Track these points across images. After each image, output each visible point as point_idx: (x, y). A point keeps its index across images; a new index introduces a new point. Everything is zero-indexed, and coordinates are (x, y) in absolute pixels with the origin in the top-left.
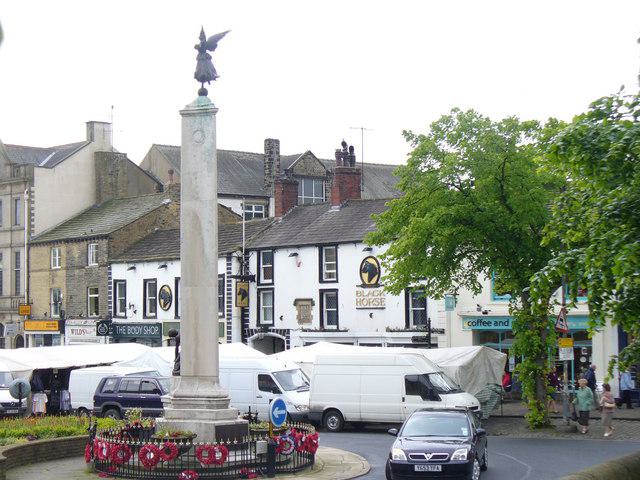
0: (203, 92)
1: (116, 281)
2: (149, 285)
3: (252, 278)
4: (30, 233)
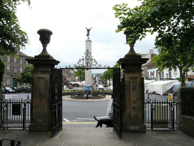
0: (88, 38)
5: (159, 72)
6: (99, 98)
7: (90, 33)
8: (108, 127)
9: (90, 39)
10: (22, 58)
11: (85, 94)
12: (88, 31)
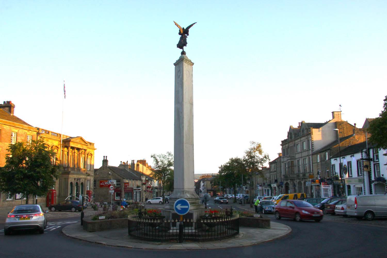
0: (183, 53)
1: (333, 166)
2: (341, 165)
3: (371, 160)
4: (312, 151)
5: (365, 163)
7: (189, 39)
8: (195, 189)
11: (174, 225)
12: (184, 33)
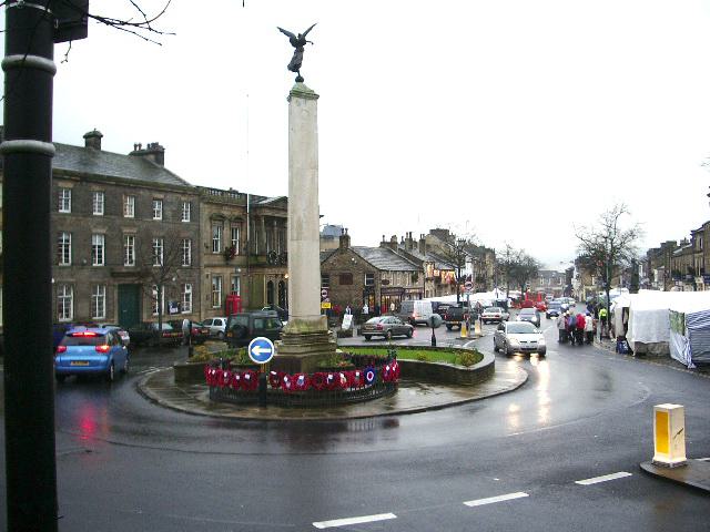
0: (300, 79)
6: (365, 401)
9: (309, 84)
10: (162, 196)
12: (299, 43)
